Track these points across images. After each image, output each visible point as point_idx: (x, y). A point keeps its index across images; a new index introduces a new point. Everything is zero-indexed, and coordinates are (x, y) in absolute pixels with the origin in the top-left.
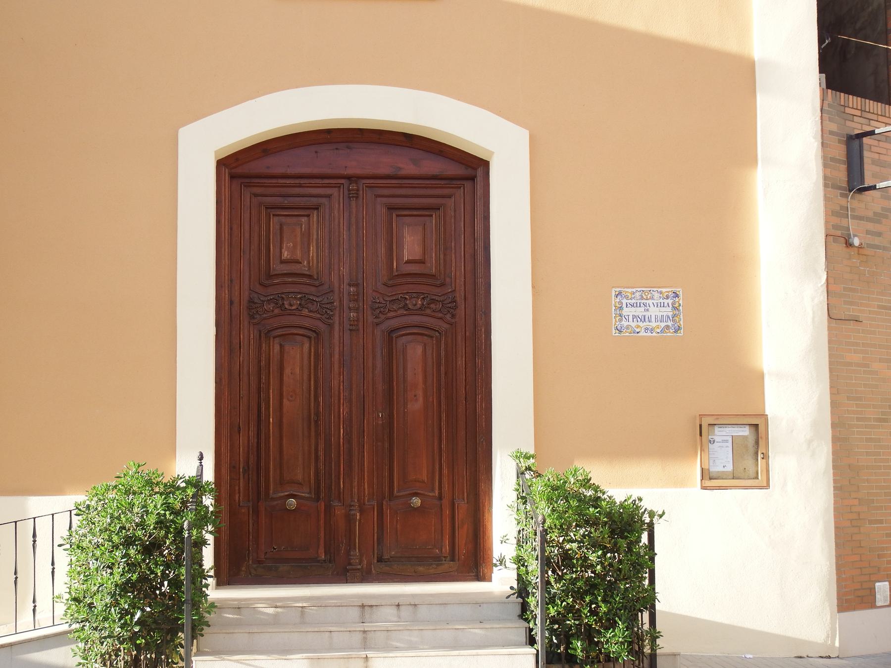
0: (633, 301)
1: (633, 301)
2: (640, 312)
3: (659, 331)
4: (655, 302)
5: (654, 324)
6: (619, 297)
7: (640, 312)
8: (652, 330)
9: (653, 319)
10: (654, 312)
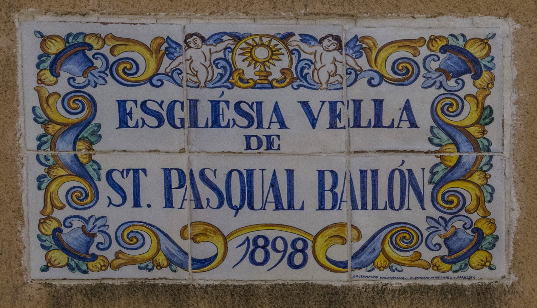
0: (169, 92)
1: (169, 92)
2: (220, 150)
3: (340, 253)
4: (315, 98)
5: (309, 219)
6: (72, 67)
7: (220, 150)
8: (297, 251)
9: (306, 190)
10: (309, 151)
